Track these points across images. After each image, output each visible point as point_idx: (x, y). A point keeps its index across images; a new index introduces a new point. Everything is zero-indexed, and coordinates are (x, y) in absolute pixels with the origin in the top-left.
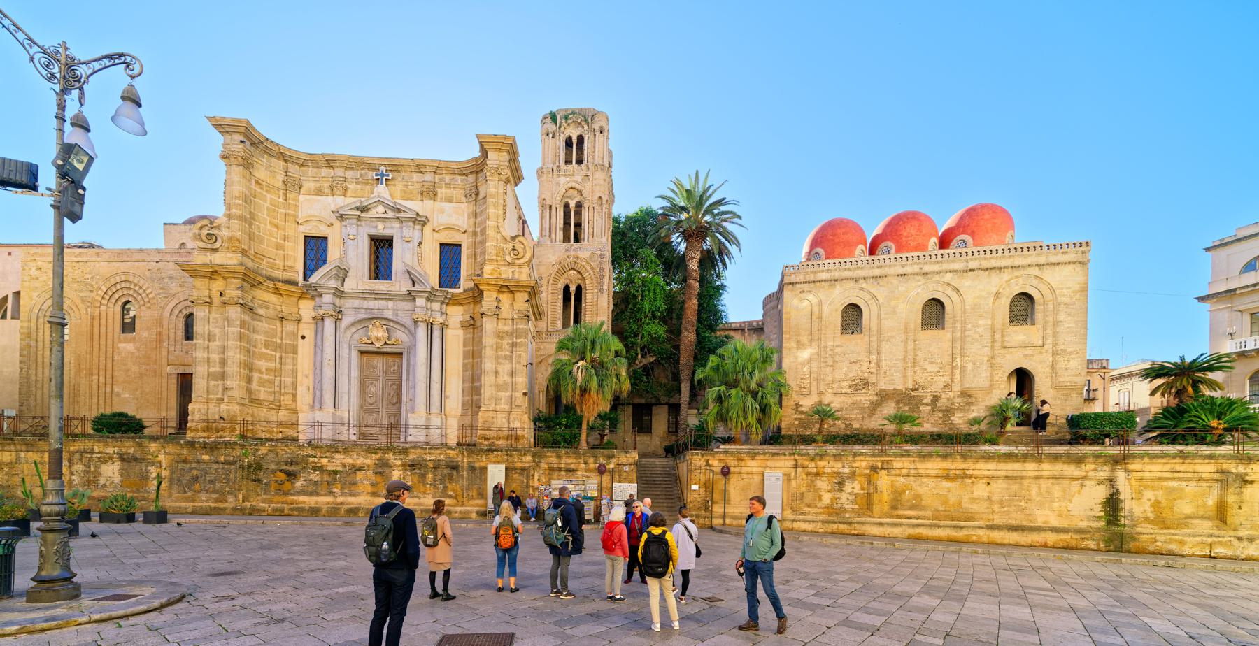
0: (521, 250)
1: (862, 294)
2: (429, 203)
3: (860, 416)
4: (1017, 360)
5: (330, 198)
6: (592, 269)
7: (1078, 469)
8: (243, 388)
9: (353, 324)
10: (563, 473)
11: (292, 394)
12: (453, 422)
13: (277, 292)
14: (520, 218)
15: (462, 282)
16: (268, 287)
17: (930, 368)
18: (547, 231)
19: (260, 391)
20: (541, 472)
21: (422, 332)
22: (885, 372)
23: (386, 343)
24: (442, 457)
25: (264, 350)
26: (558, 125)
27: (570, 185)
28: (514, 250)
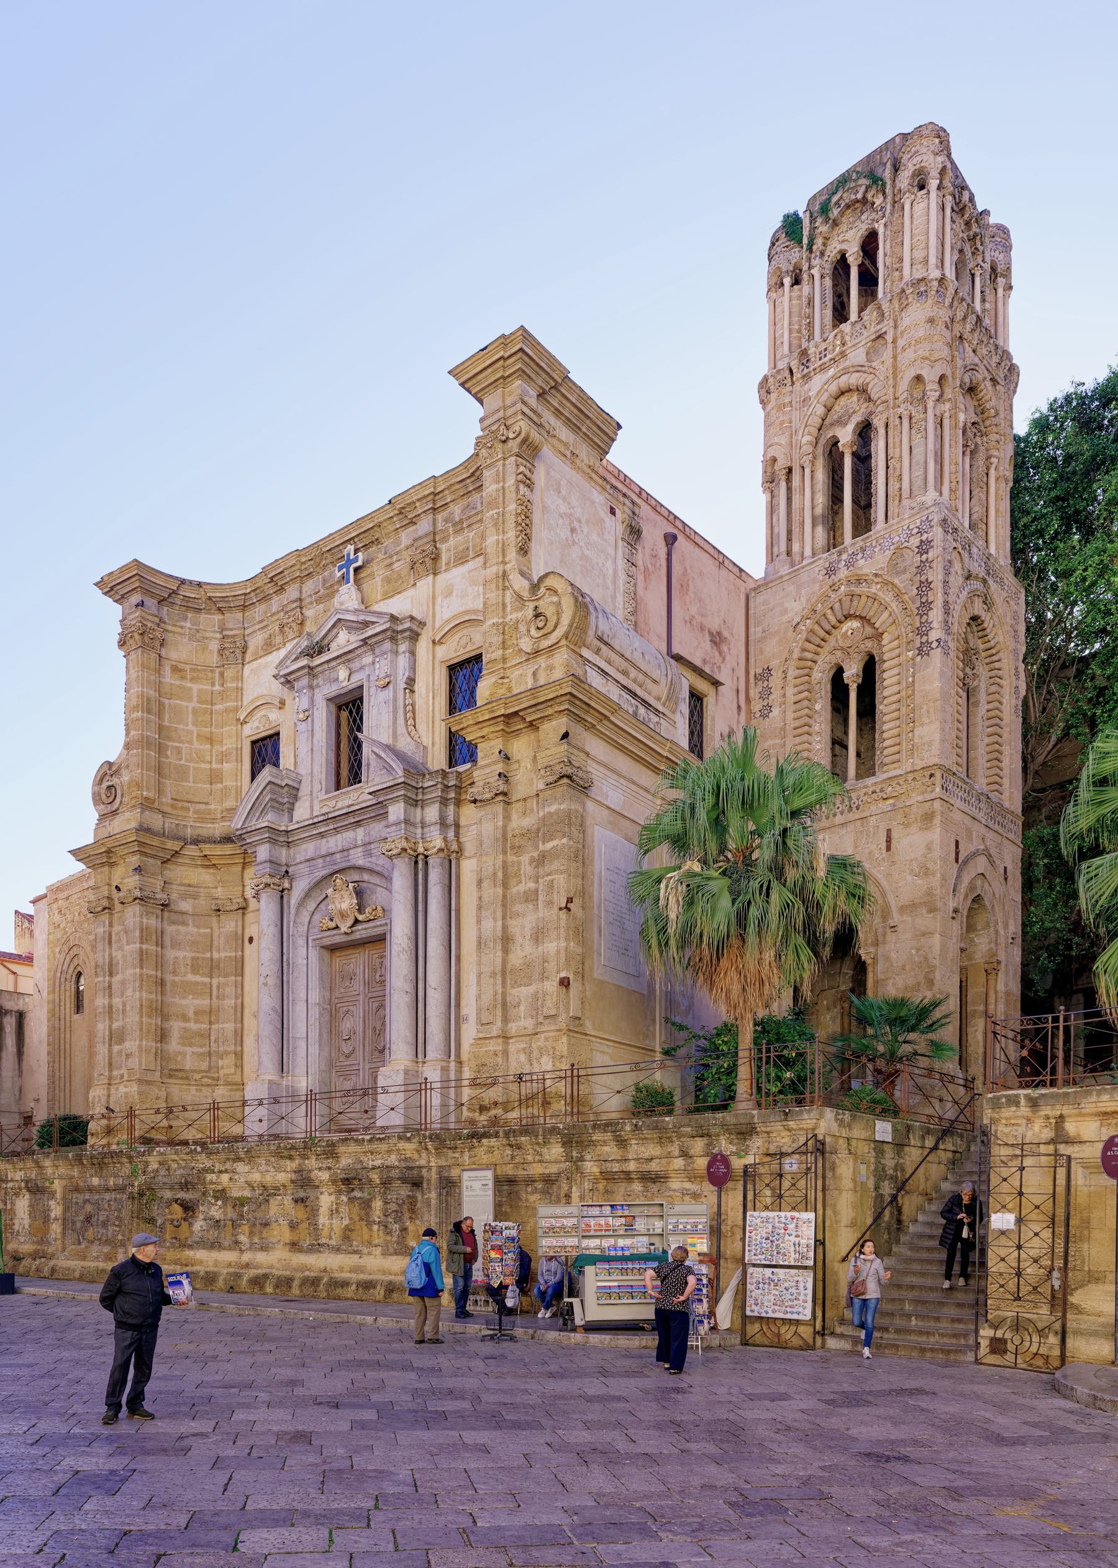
0: (549, 611)
6: (898, 595)
8: (148, 1051)
10: (637, 1187)
11: (235, 1053)
13: (208, 862)
16: (193, 858)
19: (184, 1054)
20: (587, 1185)
23: (357, 921)
24: (393, 1160)
25: (191, 977)
26: (805, 241)
27: (833, 388)
28: (537, 616)
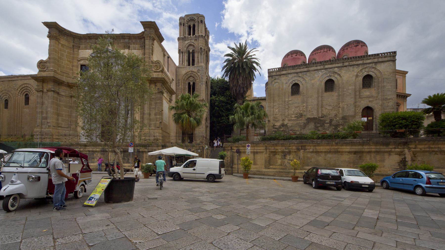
1: (300, 79)
3: (299, 129)
4: (364, 104)
7: (387, 148)
14: (164, 55)
17: (328, 108)
18: (181, 61)
22: (310, 111)
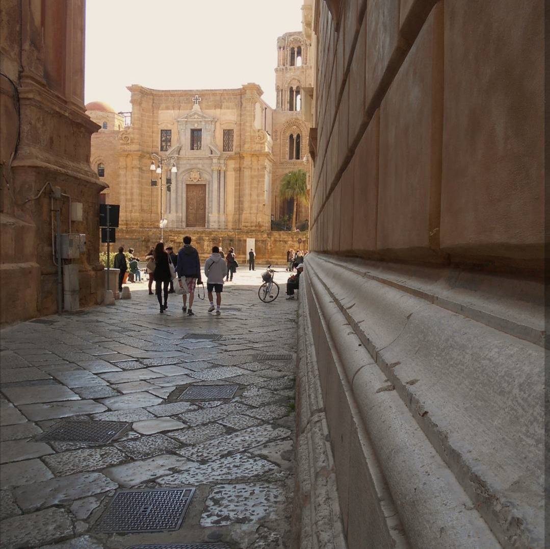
2: (218, 111)
5: (172, 111)
9: (184, 172)
12: (230, 218)
15: (234, 148)
21: (215, 175)
23: (199, 180)
28: (259, 136)
